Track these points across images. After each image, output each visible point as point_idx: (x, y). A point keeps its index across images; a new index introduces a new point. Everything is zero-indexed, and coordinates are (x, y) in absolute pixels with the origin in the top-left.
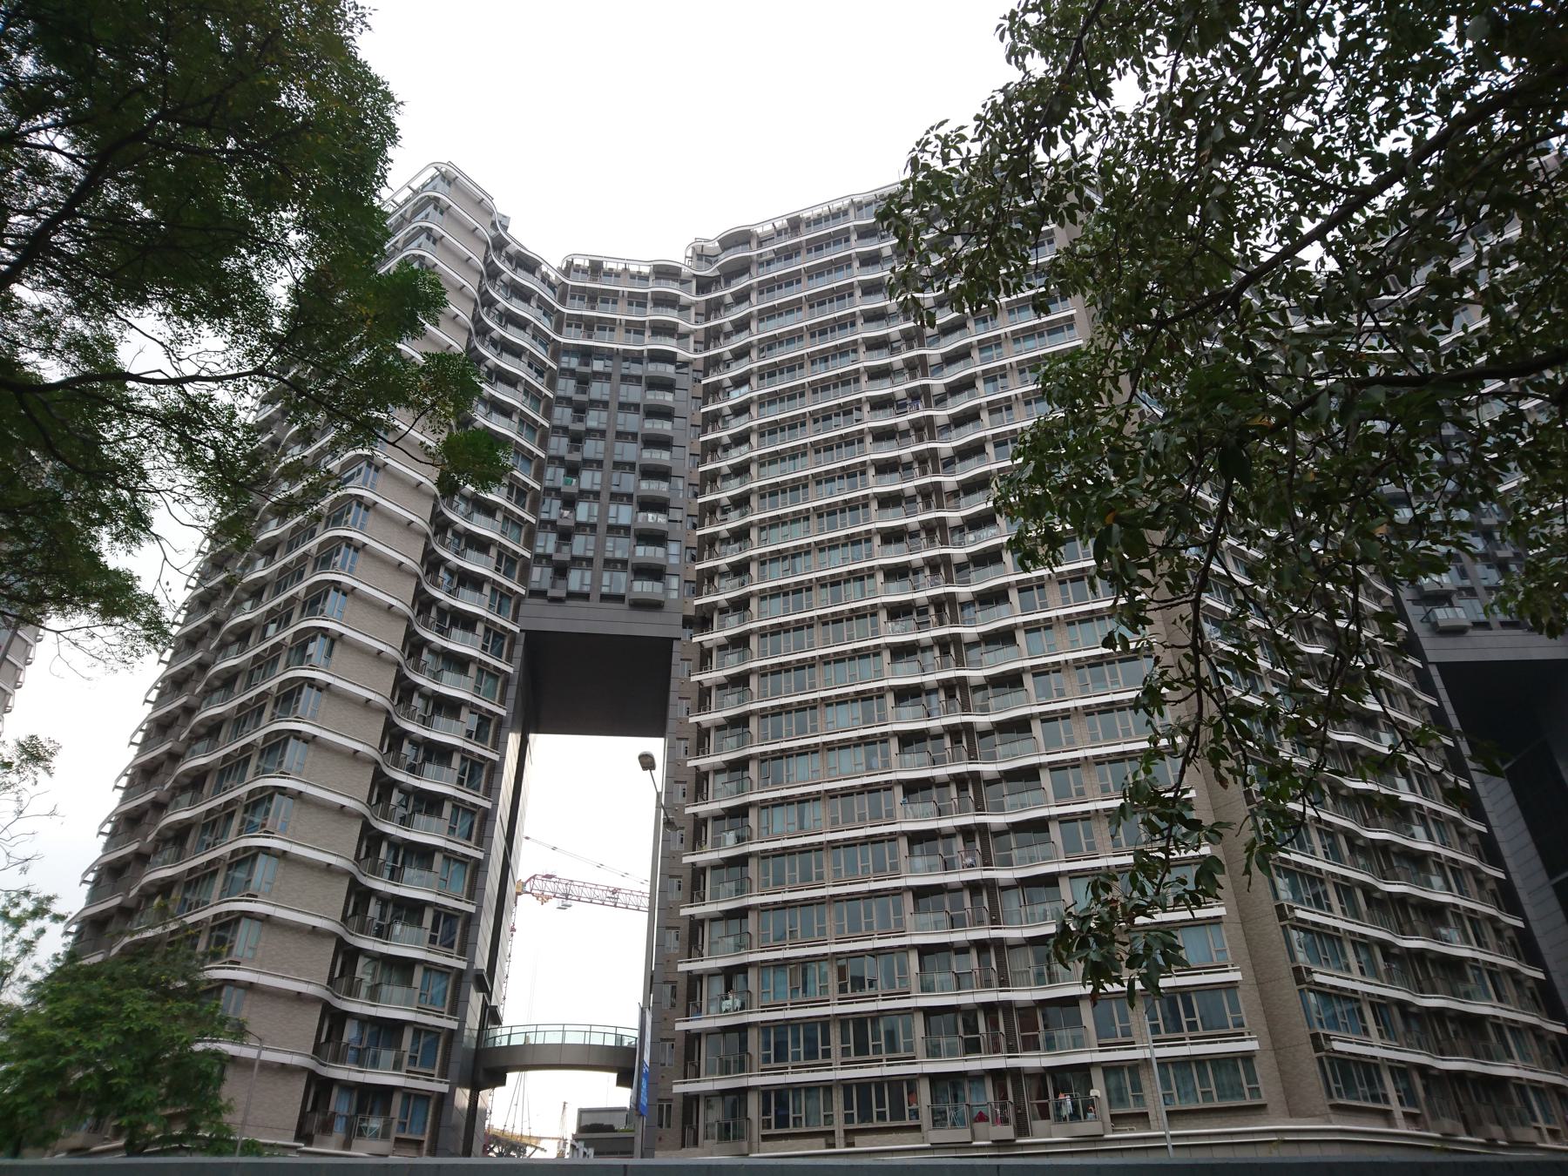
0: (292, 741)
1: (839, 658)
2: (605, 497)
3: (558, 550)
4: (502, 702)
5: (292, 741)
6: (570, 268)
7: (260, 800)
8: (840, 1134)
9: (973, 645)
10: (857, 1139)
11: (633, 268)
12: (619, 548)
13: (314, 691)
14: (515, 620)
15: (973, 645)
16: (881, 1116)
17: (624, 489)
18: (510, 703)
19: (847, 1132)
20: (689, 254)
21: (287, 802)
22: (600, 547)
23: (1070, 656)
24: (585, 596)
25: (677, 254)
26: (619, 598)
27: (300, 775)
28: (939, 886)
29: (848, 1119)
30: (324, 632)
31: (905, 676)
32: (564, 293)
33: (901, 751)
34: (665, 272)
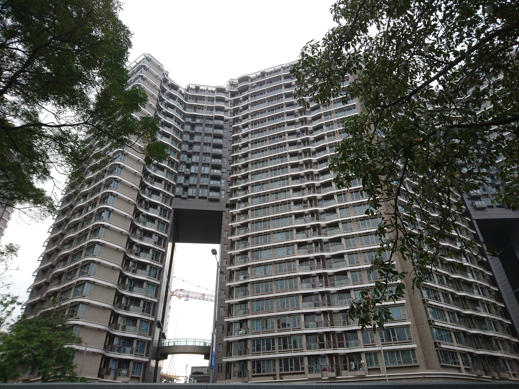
1: (278, 218)
2: (200, 164)
3: (185, 182)
4: (166, 232)
8: (278, 375)
9: (322, 213)
10: (284, 377)
11: (210, 89)
12: (205, 181)
14: (170, 205)
15: (322, 213)
16: (292, 369)
17: (206, 162)
18: (169, 232)
19: (280, 374)
20: (228, 84)
22: (199, 181)
24: (194, 197)
25: (224, 84)
26: (205, 198)
28: (311, 293)
29: (281, 370)
31: (300, 224)
32: (187, 97)
33: (298, 249)
34: (220, 90)
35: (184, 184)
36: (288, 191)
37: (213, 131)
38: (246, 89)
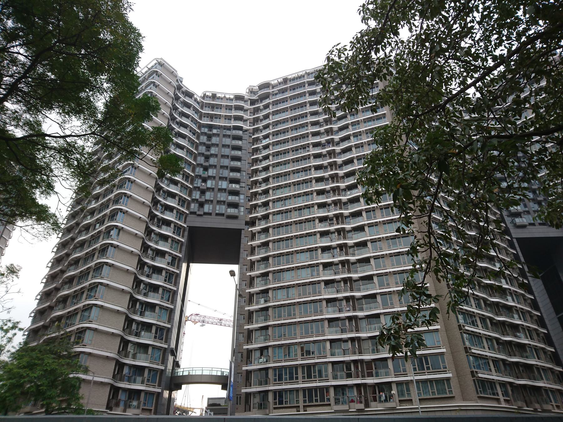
0: (105, 266)
1: (301, 236)
2: (217, 178)
3: (200, 197)
4: (180, 252)
5: (105, 266)
6: (205, 96)
7: (93, 287)
8: (301, 407)
10: (308, 409)
11: (227, 96)
12: (222, 197)
13: (113, 248)
14: (185, 222)
16: (316, 401)
18: (183, 252)
19: (304, 406)
21: (103, 288)
22: (216, 196)
23: (384, 236)
24: (210, 214)
25: (243, 91)
26: (222, 215)
27: (108, 278)
28: (337, 318)
29: (305, 401)
30: (116, 227)
31: (325, 242)
32: (202, 105)
33: (324, 270)
34: (239, 98)
35: (200, 200)
36: (313, 207)
37: (231, 143)
38: (267, 96)
